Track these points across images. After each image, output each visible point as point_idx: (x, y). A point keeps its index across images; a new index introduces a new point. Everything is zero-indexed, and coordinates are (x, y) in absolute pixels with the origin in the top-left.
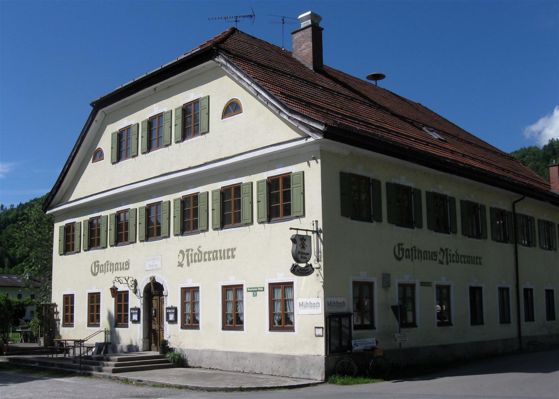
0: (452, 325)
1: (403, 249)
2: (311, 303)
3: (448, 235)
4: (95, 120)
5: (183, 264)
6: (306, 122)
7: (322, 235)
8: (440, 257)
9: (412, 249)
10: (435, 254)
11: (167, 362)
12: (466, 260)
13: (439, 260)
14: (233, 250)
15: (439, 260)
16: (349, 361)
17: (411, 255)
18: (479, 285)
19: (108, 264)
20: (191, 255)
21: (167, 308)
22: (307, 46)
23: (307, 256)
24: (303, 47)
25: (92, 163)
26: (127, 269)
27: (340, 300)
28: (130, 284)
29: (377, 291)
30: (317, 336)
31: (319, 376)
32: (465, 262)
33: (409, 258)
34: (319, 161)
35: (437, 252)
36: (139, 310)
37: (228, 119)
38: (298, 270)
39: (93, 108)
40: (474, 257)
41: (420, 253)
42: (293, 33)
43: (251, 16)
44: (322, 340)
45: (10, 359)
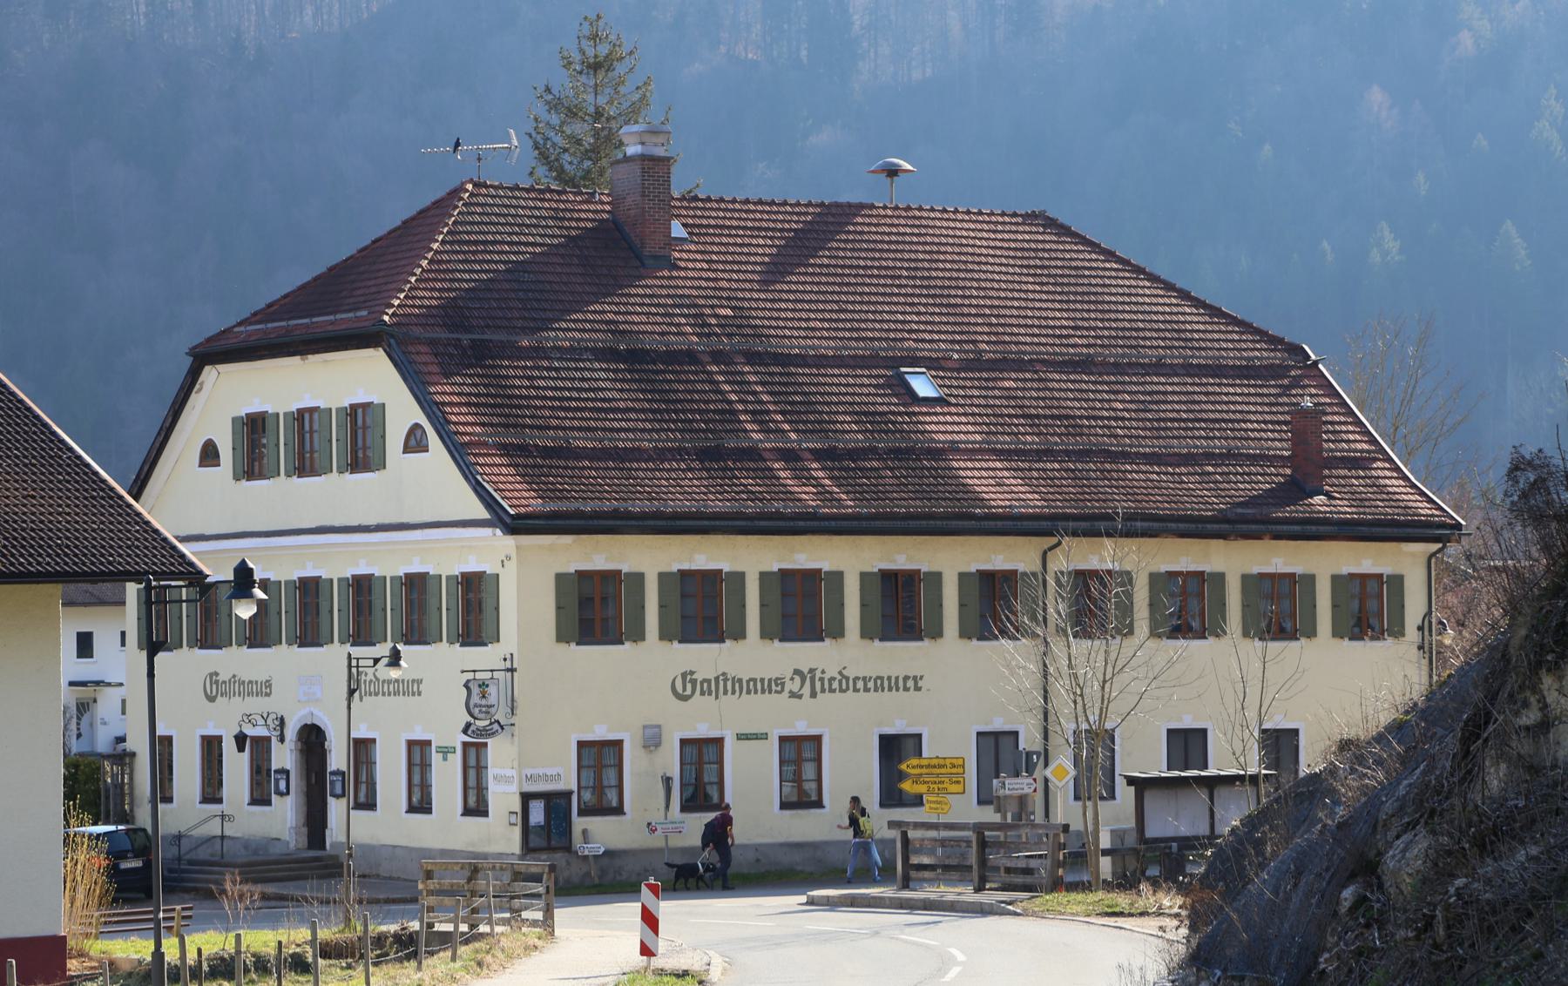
0: (824, 807)
8: (795, 686)
9: (717, 679)
10: (780, 682)
12: (871, 685)
13: (791, 692)
14: (419, 682)
19: (235, 682)
20: (822, 679)
21: (331, 773)
26: (268, 695)
28: (272, 726)
29: (632, 757)
30: (511, 824)
32: (867, 690)
36: (287, 772)
38: (473, 731)
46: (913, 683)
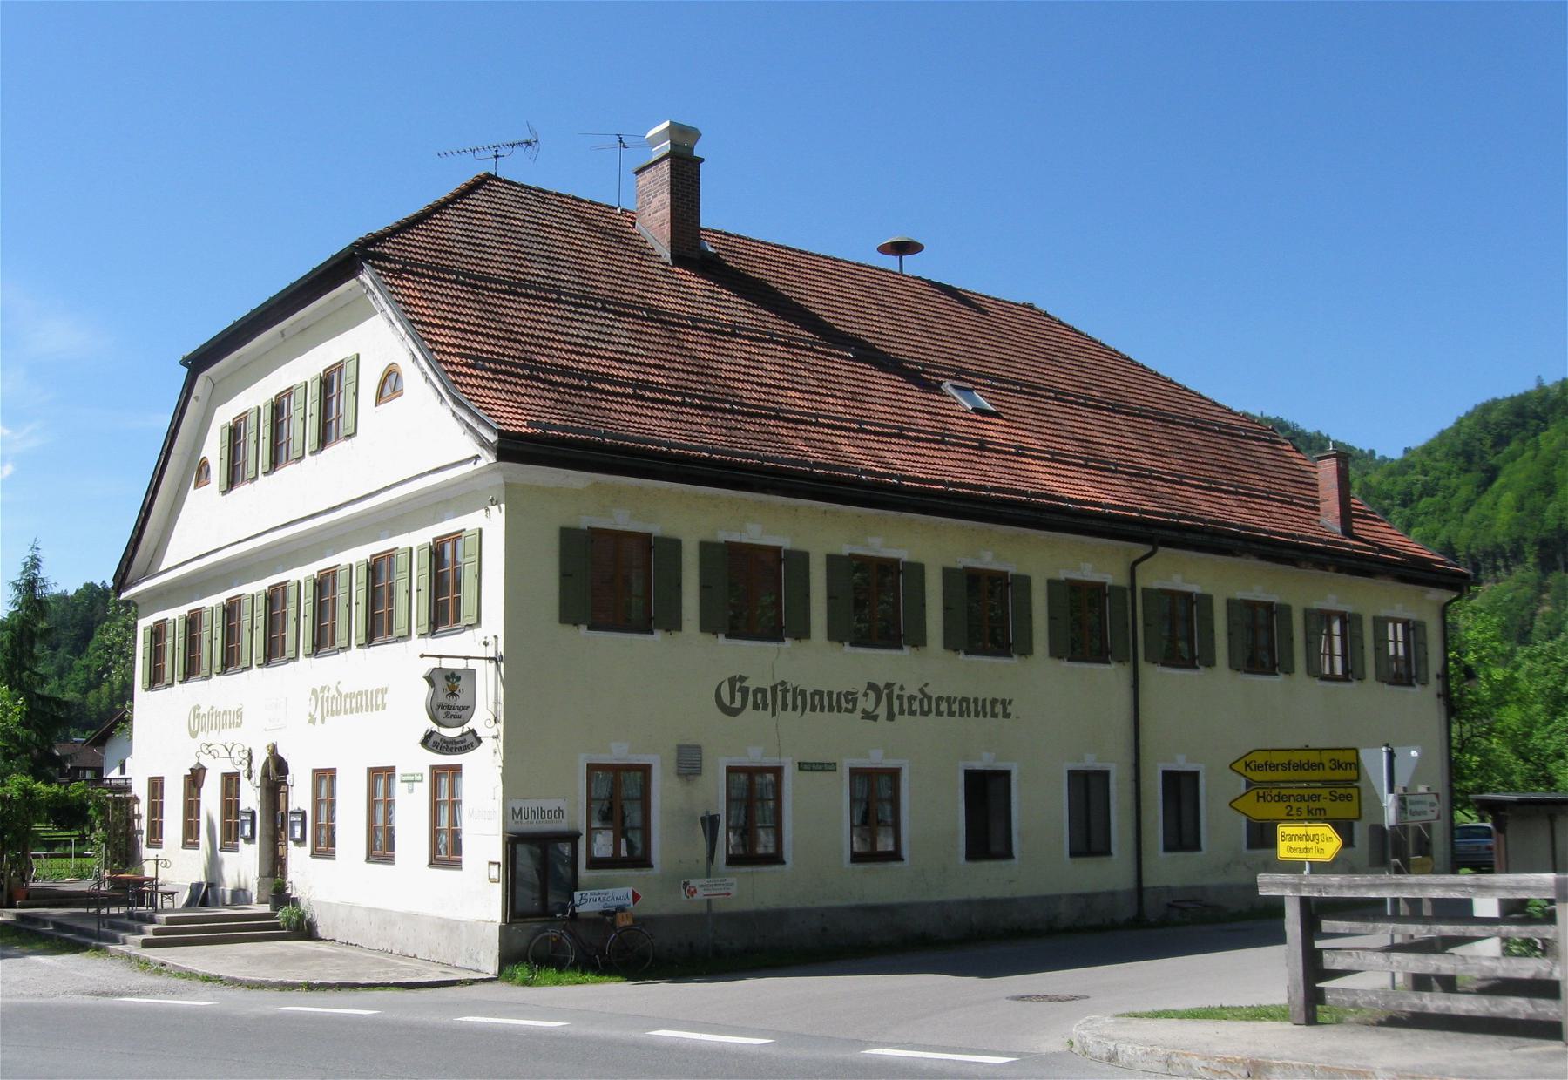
1: (745, 691)
2: (542, 811)
3: (899, 652)
4: (193, 396)
5: (877, 716)
6: (474, 424)
7: (502, 665)
8: (868, 703)
9: (774, 689)
10: (850, 697)
11: (277, 927)
12: (955, 707)
13: (864, 711)
15: (864, 711)
16: (558, 936)
17: (769, 701)
18: (1001, 766)
22: (662, 203)
23: (463, 713)
24: (655, 203)
25: (195, 488)
26: (239, 725)
27: (550, 805)
28: (238, 759)
31: (491, 968)
32: (951, 714)
33: (765, 708)
34: (503, 506)
35: (856, 693)
36: (253, 814)
37: (384, 407)
39: (187, 370)
40: (984, 701)
41: (799, 698)
42: (638, 172)
43: (529, 143)
44: (498, 888)
45: (17, 915)
46: (999, 708)
